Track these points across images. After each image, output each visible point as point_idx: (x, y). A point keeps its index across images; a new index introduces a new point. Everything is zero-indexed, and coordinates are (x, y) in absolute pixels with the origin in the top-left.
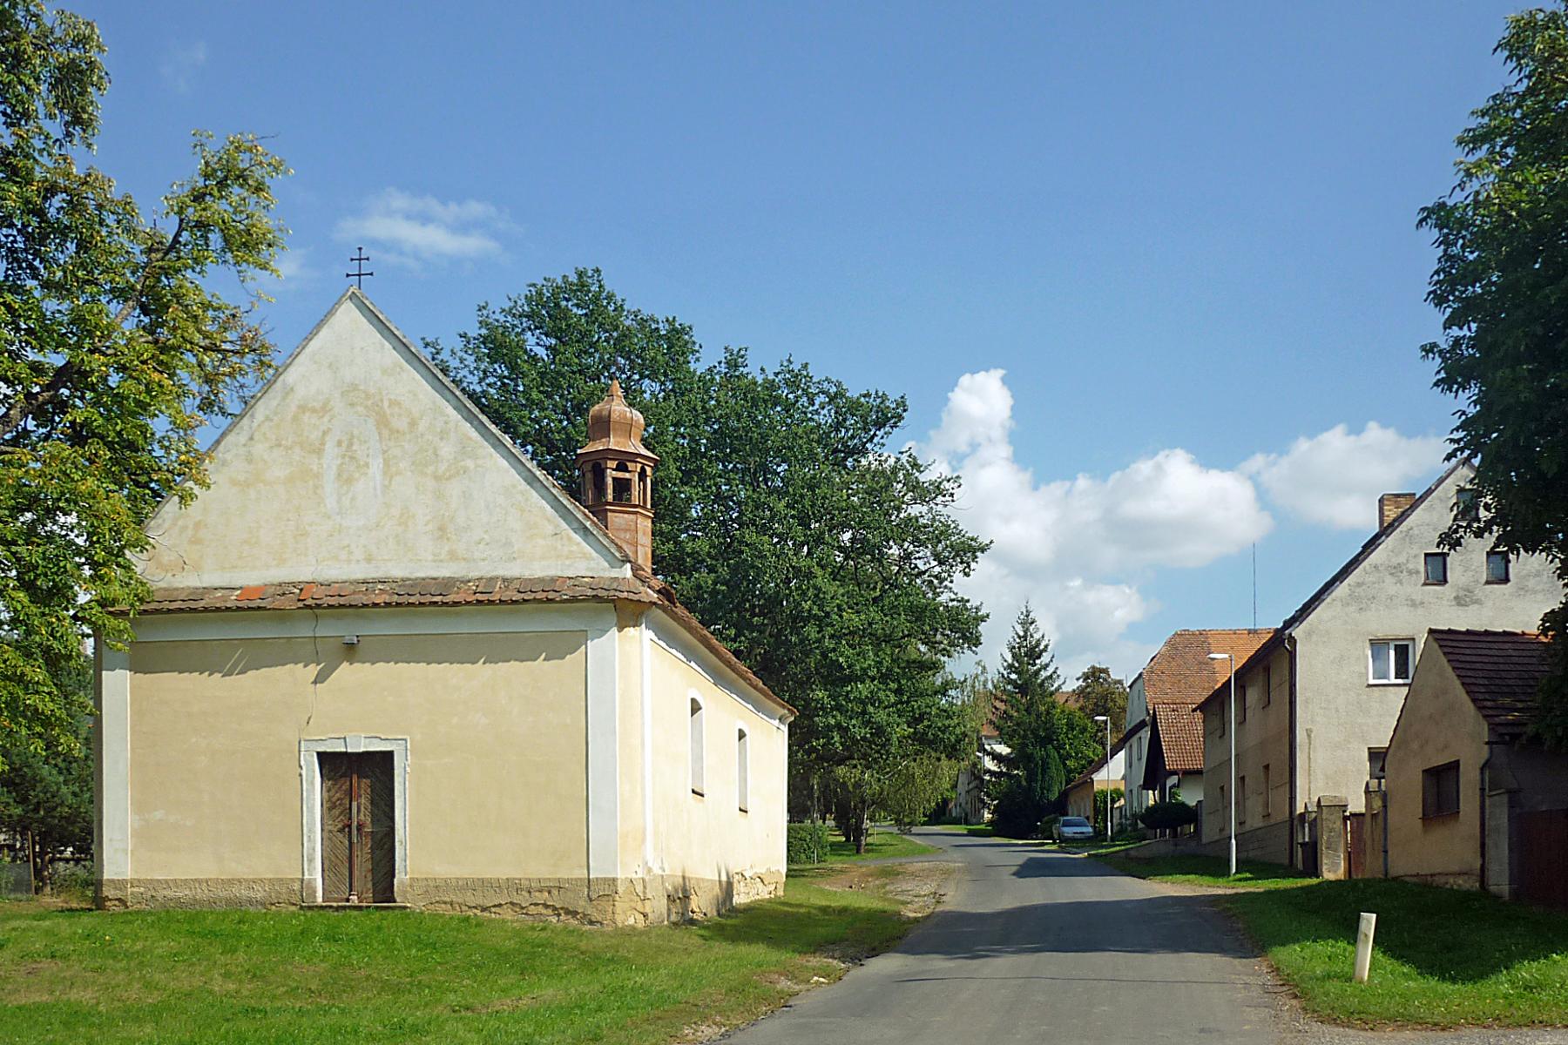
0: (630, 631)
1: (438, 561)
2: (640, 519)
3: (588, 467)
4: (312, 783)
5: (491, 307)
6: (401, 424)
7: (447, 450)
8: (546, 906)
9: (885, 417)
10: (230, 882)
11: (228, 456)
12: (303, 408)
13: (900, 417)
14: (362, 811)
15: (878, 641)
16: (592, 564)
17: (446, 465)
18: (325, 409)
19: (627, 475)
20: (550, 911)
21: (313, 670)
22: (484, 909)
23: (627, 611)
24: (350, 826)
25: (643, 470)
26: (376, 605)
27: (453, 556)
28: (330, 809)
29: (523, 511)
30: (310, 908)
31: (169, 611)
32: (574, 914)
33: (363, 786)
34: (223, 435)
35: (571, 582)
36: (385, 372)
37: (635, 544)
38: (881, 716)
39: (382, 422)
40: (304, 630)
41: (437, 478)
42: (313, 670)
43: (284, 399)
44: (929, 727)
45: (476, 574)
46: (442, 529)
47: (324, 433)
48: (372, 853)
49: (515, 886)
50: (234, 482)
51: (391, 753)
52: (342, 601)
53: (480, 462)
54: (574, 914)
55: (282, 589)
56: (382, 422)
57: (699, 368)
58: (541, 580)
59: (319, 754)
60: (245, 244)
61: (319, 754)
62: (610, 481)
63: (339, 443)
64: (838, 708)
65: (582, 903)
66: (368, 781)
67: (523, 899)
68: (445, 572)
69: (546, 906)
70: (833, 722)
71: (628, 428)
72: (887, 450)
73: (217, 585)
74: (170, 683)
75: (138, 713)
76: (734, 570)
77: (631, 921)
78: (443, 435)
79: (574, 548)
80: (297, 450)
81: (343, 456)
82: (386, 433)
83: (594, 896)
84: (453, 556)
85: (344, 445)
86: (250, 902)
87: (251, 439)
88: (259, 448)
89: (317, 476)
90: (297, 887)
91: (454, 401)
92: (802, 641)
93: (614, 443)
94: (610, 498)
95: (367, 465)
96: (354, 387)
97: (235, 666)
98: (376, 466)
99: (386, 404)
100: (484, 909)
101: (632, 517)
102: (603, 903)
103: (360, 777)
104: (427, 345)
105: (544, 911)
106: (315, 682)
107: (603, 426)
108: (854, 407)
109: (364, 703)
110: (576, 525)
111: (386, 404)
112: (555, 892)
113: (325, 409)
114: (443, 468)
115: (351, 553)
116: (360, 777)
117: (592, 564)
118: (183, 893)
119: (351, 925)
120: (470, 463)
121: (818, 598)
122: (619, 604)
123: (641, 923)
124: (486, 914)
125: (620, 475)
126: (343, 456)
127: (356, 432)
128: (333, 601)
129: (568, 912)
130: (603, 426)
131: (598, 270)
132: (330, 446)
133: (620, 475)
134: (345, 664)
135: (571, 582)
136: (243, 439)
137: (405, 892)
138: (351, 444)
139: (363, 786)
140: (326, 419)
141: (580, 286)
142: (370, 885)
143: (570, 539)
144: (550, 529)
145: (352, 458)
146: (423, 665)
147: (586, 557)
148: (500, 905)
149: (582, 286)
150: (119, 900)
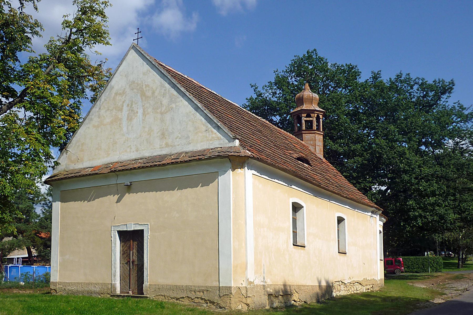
0: (239, 171)
1: (161, 148)
2: (317, 136)
3: (295, 117)
4: (115, 244)
5: (279, 71)
6: (149, 94)
7: (165, 101)
8: (202, 299)
9: (445, 89)
10: (89, 284)
11: (93, 117)
12: (116, 94)
13: (451, 89)
14: (134, 256)
15: (439, 178)
16: (221, 142)
17: (165, 107)
18: (124, 93)
19: (311, 119)
20: (203, 301)
21: (116, 197)
22: (177, 299)
23: (237, 161)
24: (129, 261)
25: (318, 117)
26: (135, 168)
27: (167, 145)
28: (123, 254)
29: (193, 122)
30: (114, 296)
31: (69, 178)
32: (213, 303)
33: (134, 245)
34: (91, 109)
35: (211, 151)
36: (144, 74)
37: (315, 145)
38: (442, 211)
39: (143, 94)
40: (113, 181)
41: (162, 113)
42: (116, 197)
43: (110, 92)
44: (469, 214)
45: (176, 152)
46: (163, 134)
47: (123, 102)
48: (138, 273)
49: (189, 289)
50: (94, 126)
51: (143, 230)
52: (123, 168)
53: (177, 104)
54: (213, 303)
55: (106, 166)
56: (143, 94)
57: (361, 80)
58: (200, 151)
59: (119, 232)
60: (98, 35)
61: (119, 232)
62: (303, 122)
63: (128, 105)
64: (420, 208)
65: (216, 298)
66: (136, 243)
67: (192, 295)
68: (164, 152)
69: (202, 299)
70: (417, 214)
71: (311, 100)
72: (449, 101)
73: (88, 167)
74: (72, 205)
75: (63, 217)
76: (371, 154)
77: (240, 307)
78: (164, 95)
79: (214, 135)
80: (114, 110)
81: (129, 111)
82: (144, 98)
83: (221, 295)
84: (167, 145)
85: (130, 105)
86: (95, 293)
87: (100, 109)
88: (102, 112)
89: (121, 119)
90: (110, 287)
91: (168, 80)
92: (401, 181)
93: (305, 107)
94: (304, 128)
95: (137, 112)
96: (133, 82)
97: (91, 198)
98: (140, 111)
99: (144, 87)
100: (177, 299)
101: (314, 135)
102: (226, 299)
103: (132, 240)
104: (252, 86)
105: (201, 301)
106: (117, 202)
107: (301, 101)
108: (431, 88)
109: (134, 209)
110: (214, 125)
111: (144, 87)
112: (205, 292)
113: (124, 93)
114: (163, 109)
115: (131, 148)
116: (132, 240)
117: (221, 142)
118: (74, 288)
119: (131, 302)
120: (173, 105)
121: (409, 165)
122: (230, 158)
123: (245, 308)
124: (178, 301)
125: (308, 119)
126: (129, 111)
127: (134, 100)
128: (120, 168)
129: (211, 302)
130: (301, 101)
131: (315, 50)
132: (125, 108)
133: (308, 119)
134: (127, 194)
135: (211, 151)
136: (97, 110)
137: (147, 290)
138: (132, 105)
139: (134, 245)
140: (124, 97)
141: (309, 57)
142: (136, 287)
143: (212, 132)
144: (204, 128)
145: (132, 110)
146: (154, 192)
147: (219, 139)
148: (183, 298)
149: (310, 57)
150: (54, 290)
